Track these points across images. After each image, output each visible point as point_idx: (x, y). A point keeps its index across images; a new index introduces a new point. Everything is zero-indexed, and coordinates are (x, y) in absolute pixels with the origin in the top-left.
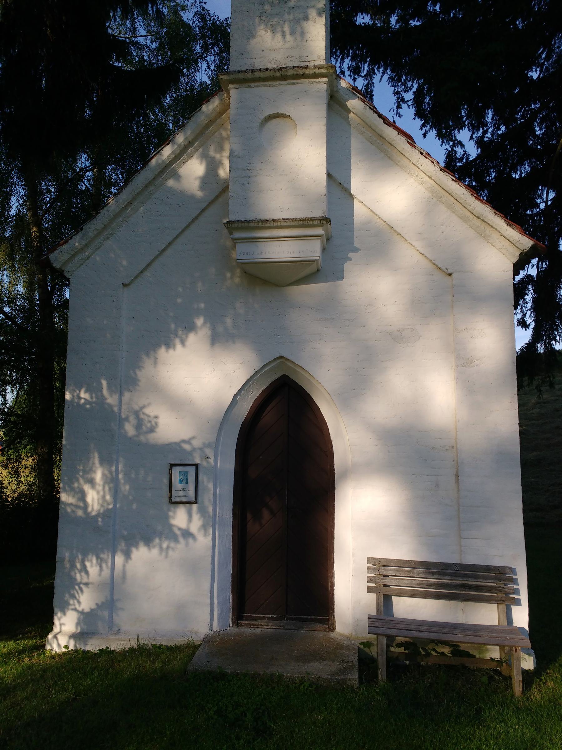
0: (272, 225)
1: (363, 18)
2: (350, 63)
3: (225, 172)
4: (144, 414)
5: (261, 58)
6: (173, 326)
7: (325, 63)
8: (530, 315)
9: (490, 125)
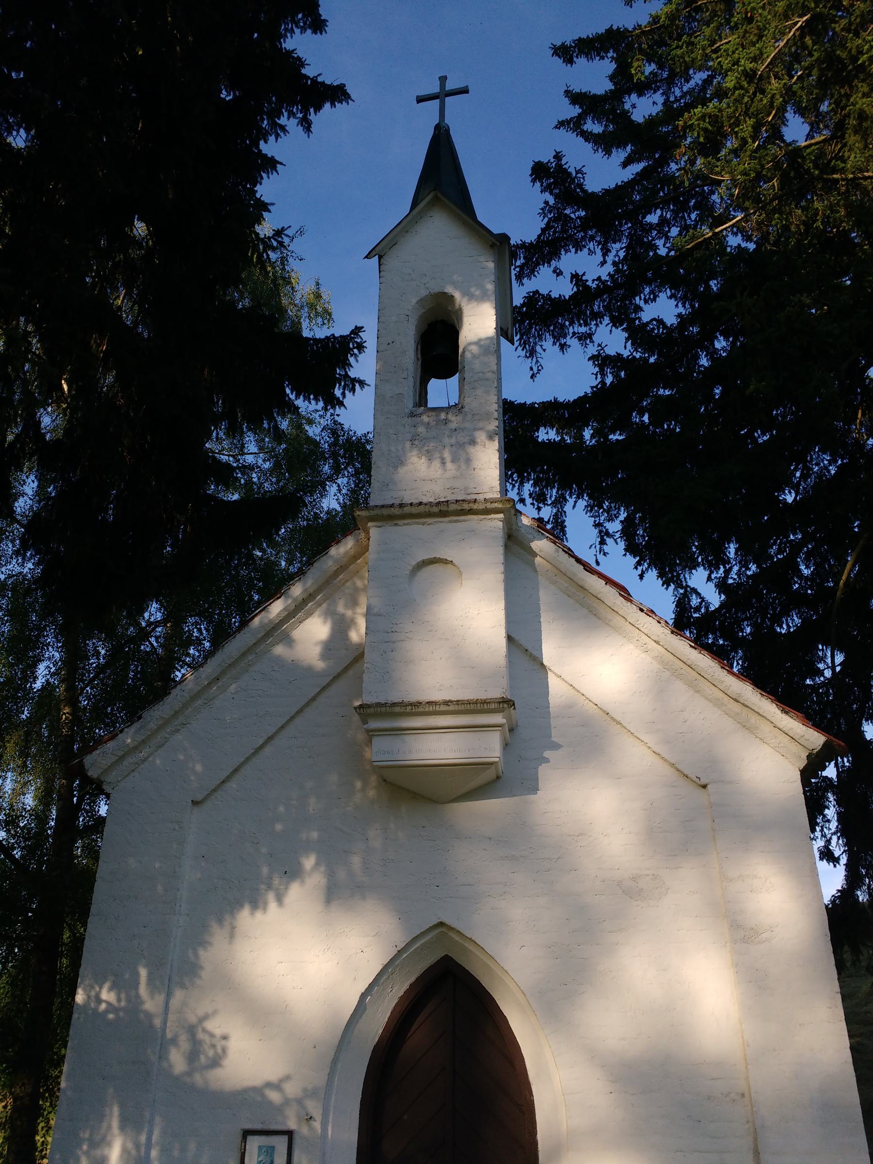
0: (427, 709)
1: (547, 433)
2: (532, 489)
3: (359, 635)
4: (205, 1031)
5: (412, 489)
7: (499, 496)
8: (838, 843)
9: (734, 562)
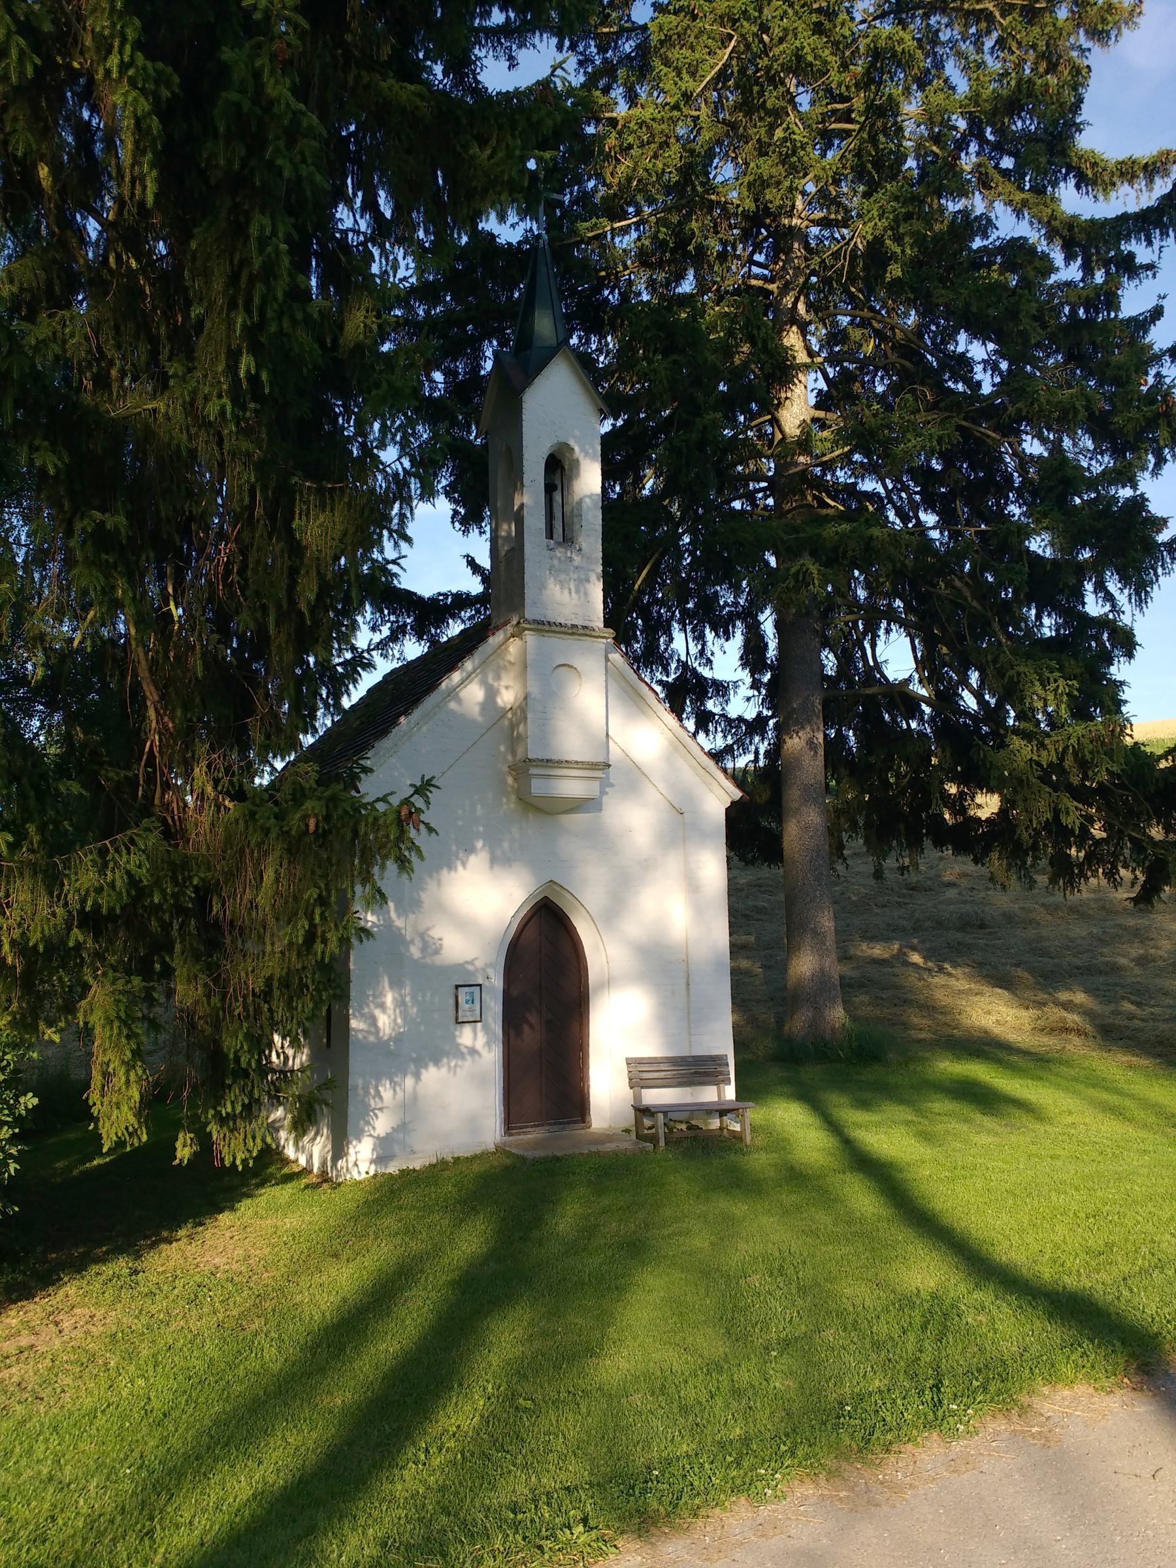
6: (454, 848)
